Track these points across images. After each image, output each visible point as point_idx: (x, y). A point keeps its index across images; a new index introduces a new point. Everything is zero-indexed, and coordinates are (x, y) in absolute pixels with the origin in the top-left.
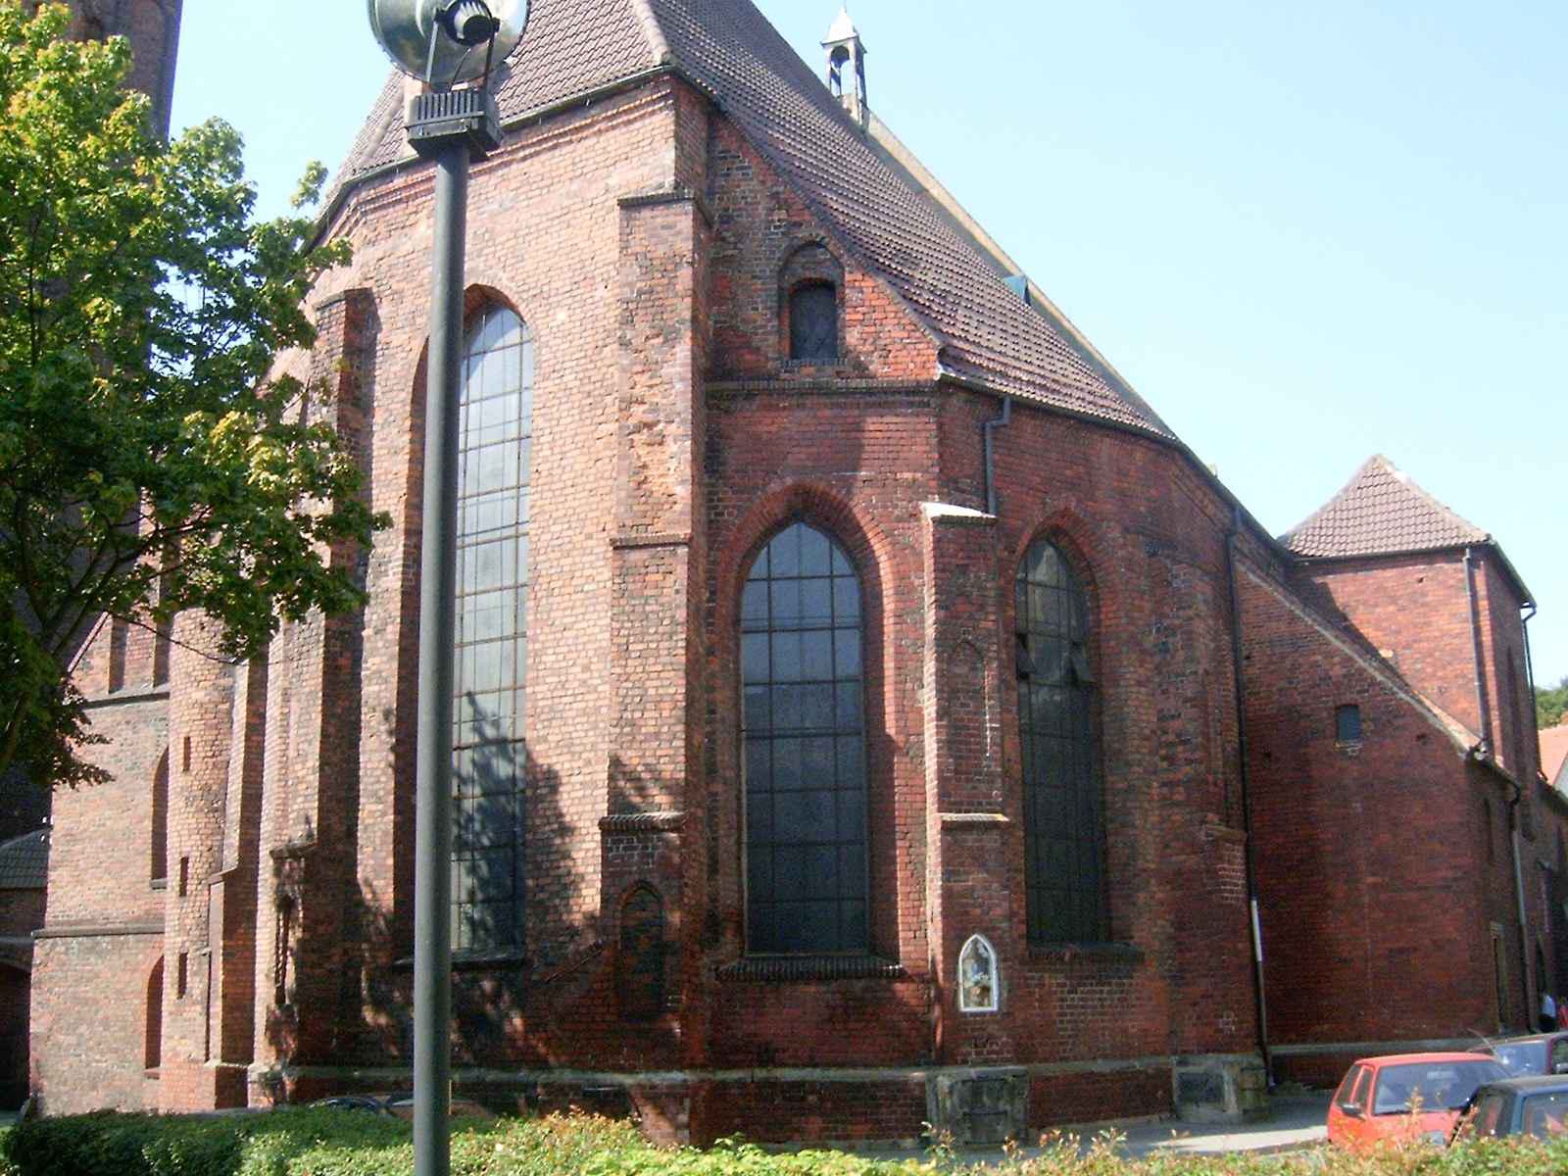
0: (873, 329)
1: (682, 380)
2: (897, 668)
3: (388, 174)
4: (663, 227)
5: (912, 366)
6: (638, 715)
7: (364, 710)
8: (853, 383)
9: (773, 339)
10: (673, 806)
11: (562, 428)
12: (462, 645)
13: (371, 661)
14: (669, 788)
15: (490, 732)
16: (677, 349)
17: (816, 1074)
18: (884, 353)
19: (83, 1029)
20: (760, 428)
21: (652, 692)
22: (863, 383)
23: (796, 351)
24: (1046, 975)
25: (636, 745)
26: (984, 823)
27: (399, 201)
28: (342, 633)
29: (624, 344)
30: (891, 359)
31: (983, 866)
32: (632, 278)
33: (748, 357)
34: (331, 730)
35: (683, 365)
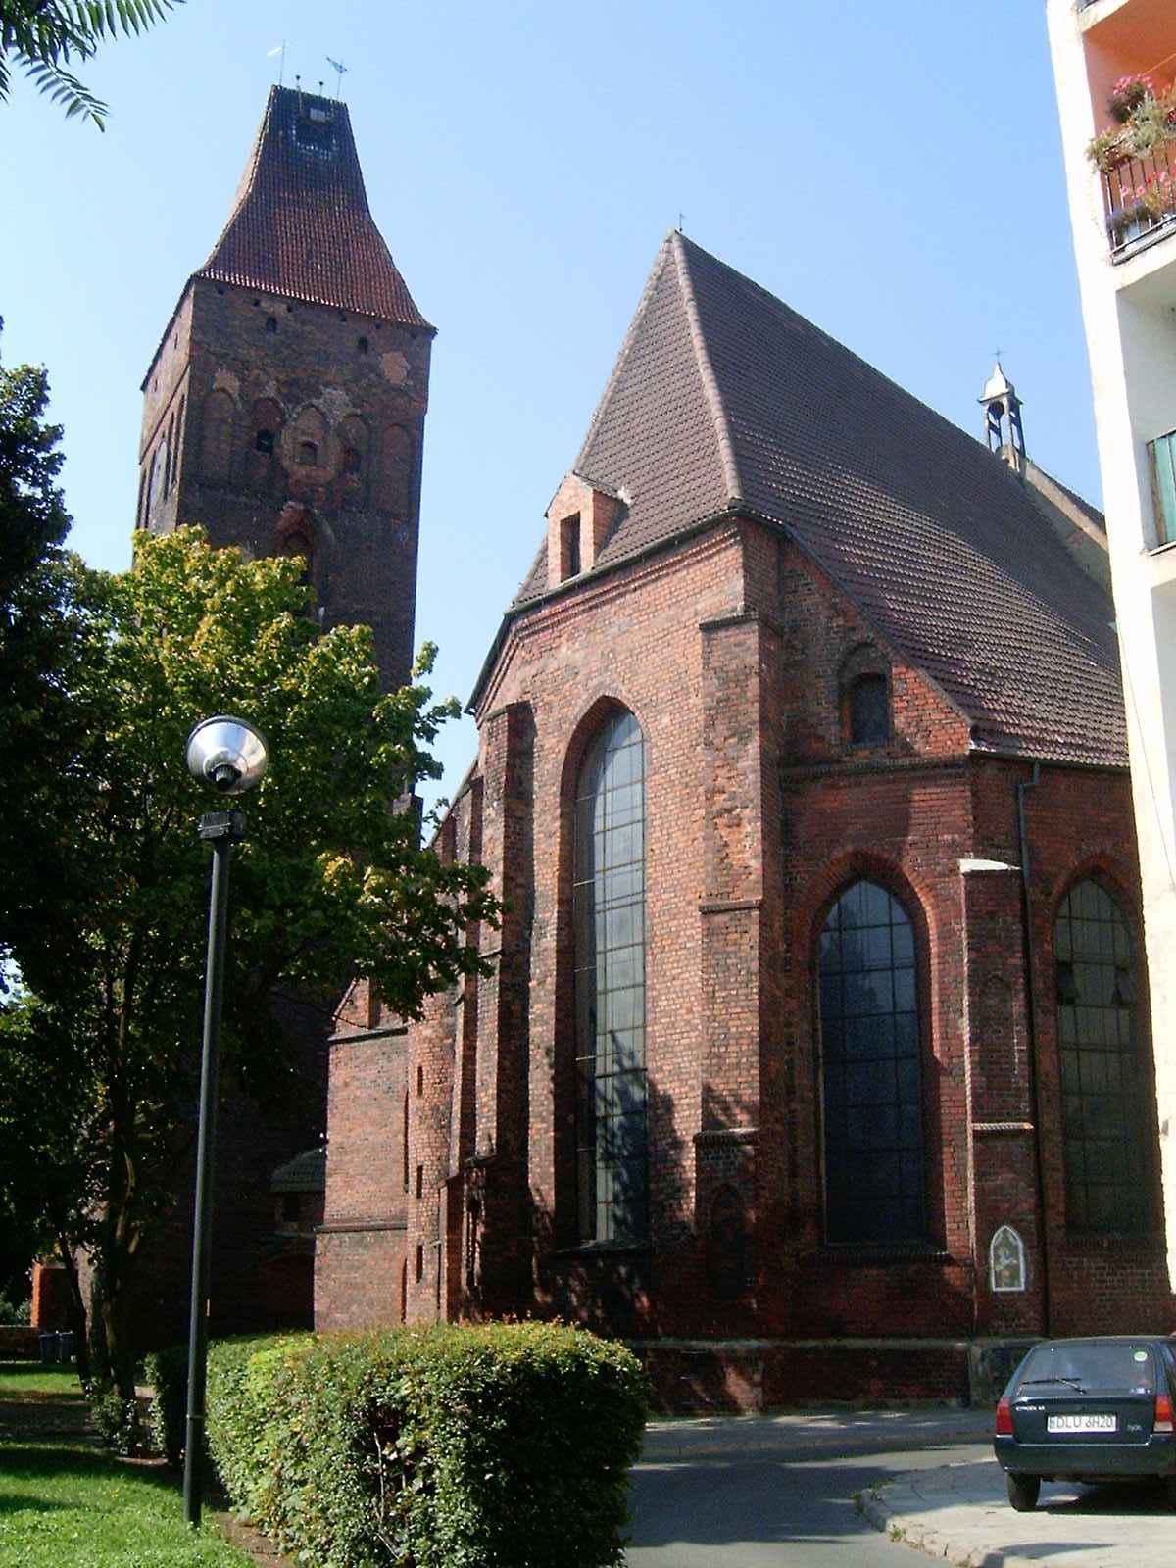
0: (916, 714)
1: (754, 771)
2: (941, 1001)
3: (537, 606)
4: (735, 645)
5: (949, 743)
6: (723, 1049)
7: (531, 1046)
8: (900, 762)
9: (834, 729)
10: (752, 1122)
11: (667, 814)
12: (605, 992)
13: (536, 1007)
14: (746, 1109)
15: (627, 1064)
16: (749, 746)
17: (876, 1343)
18: (925, 734)
19: (354, 1308)
20: (826, 805)
21: (733, 1030)
22: (907, 761)
23: (857, 737)
24: (1085, 1260)
25: (722, 1074)
26: (1010, 1131)
27: (547, 627)
28: (513, 985)
29: (708, 744)
30: (932, 738)
31: (1011, 1168)
32: (713, 689)
33: (815, 745)
34: (507, 1064)
35: (753, 760)
